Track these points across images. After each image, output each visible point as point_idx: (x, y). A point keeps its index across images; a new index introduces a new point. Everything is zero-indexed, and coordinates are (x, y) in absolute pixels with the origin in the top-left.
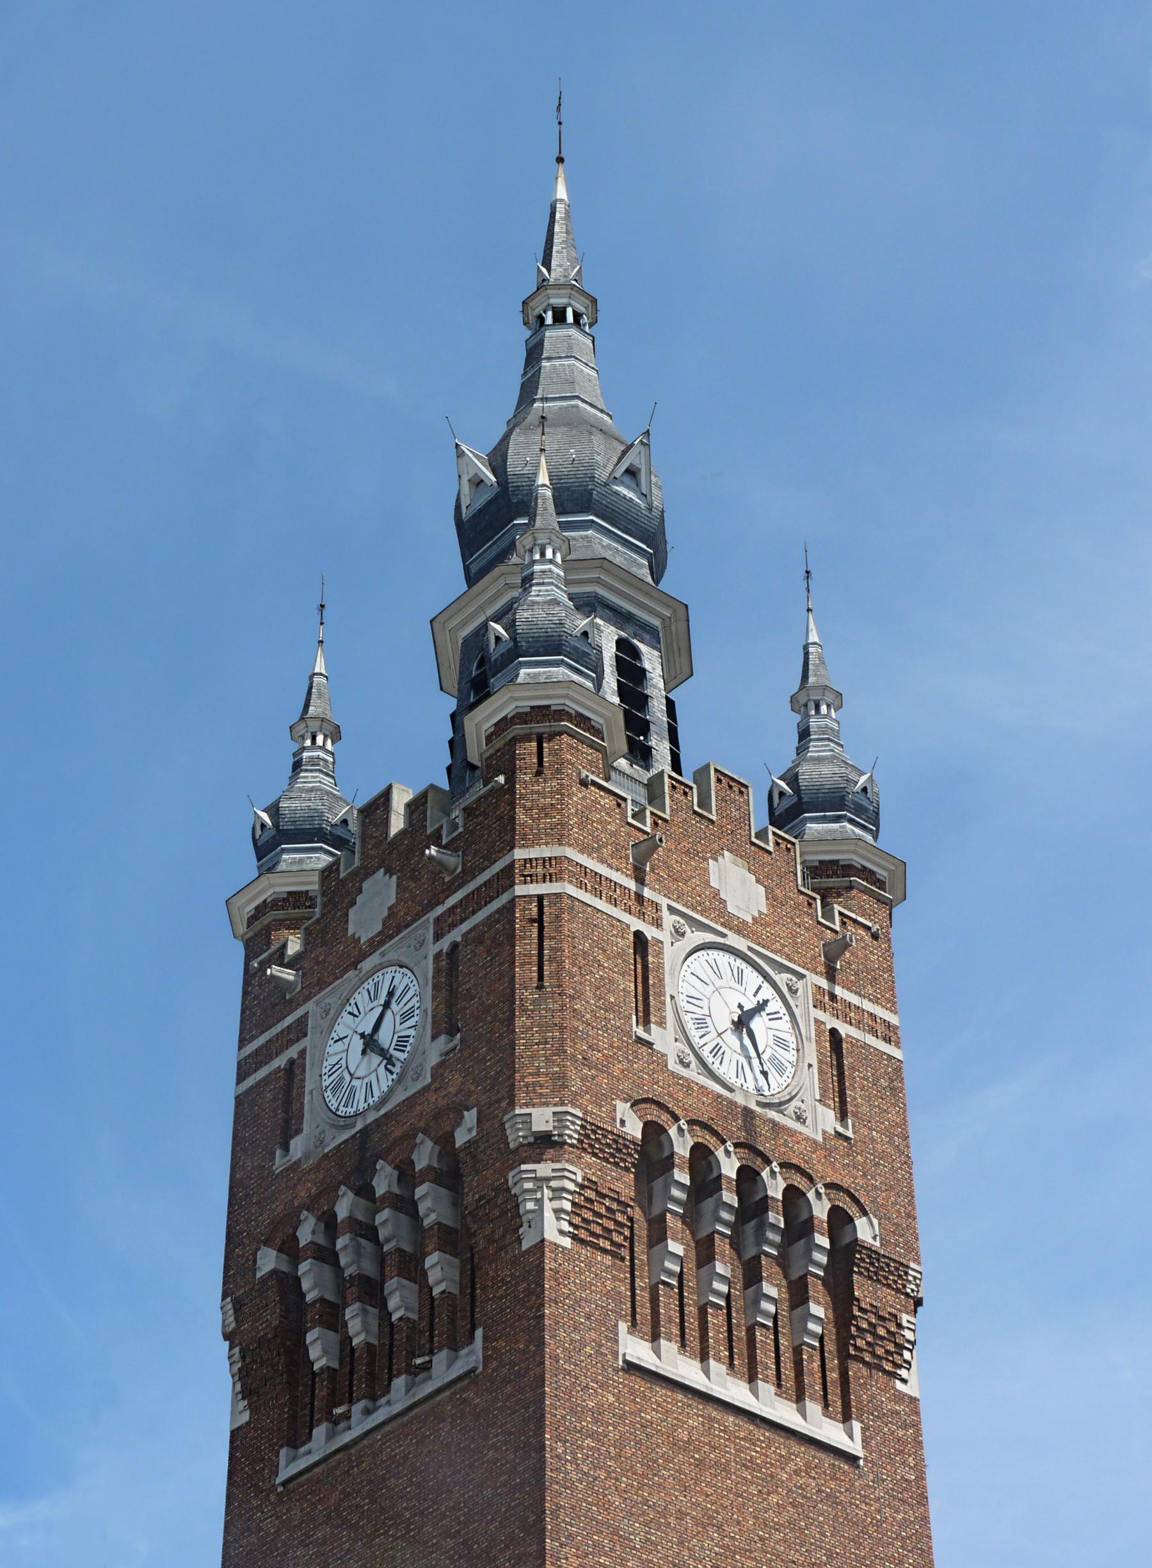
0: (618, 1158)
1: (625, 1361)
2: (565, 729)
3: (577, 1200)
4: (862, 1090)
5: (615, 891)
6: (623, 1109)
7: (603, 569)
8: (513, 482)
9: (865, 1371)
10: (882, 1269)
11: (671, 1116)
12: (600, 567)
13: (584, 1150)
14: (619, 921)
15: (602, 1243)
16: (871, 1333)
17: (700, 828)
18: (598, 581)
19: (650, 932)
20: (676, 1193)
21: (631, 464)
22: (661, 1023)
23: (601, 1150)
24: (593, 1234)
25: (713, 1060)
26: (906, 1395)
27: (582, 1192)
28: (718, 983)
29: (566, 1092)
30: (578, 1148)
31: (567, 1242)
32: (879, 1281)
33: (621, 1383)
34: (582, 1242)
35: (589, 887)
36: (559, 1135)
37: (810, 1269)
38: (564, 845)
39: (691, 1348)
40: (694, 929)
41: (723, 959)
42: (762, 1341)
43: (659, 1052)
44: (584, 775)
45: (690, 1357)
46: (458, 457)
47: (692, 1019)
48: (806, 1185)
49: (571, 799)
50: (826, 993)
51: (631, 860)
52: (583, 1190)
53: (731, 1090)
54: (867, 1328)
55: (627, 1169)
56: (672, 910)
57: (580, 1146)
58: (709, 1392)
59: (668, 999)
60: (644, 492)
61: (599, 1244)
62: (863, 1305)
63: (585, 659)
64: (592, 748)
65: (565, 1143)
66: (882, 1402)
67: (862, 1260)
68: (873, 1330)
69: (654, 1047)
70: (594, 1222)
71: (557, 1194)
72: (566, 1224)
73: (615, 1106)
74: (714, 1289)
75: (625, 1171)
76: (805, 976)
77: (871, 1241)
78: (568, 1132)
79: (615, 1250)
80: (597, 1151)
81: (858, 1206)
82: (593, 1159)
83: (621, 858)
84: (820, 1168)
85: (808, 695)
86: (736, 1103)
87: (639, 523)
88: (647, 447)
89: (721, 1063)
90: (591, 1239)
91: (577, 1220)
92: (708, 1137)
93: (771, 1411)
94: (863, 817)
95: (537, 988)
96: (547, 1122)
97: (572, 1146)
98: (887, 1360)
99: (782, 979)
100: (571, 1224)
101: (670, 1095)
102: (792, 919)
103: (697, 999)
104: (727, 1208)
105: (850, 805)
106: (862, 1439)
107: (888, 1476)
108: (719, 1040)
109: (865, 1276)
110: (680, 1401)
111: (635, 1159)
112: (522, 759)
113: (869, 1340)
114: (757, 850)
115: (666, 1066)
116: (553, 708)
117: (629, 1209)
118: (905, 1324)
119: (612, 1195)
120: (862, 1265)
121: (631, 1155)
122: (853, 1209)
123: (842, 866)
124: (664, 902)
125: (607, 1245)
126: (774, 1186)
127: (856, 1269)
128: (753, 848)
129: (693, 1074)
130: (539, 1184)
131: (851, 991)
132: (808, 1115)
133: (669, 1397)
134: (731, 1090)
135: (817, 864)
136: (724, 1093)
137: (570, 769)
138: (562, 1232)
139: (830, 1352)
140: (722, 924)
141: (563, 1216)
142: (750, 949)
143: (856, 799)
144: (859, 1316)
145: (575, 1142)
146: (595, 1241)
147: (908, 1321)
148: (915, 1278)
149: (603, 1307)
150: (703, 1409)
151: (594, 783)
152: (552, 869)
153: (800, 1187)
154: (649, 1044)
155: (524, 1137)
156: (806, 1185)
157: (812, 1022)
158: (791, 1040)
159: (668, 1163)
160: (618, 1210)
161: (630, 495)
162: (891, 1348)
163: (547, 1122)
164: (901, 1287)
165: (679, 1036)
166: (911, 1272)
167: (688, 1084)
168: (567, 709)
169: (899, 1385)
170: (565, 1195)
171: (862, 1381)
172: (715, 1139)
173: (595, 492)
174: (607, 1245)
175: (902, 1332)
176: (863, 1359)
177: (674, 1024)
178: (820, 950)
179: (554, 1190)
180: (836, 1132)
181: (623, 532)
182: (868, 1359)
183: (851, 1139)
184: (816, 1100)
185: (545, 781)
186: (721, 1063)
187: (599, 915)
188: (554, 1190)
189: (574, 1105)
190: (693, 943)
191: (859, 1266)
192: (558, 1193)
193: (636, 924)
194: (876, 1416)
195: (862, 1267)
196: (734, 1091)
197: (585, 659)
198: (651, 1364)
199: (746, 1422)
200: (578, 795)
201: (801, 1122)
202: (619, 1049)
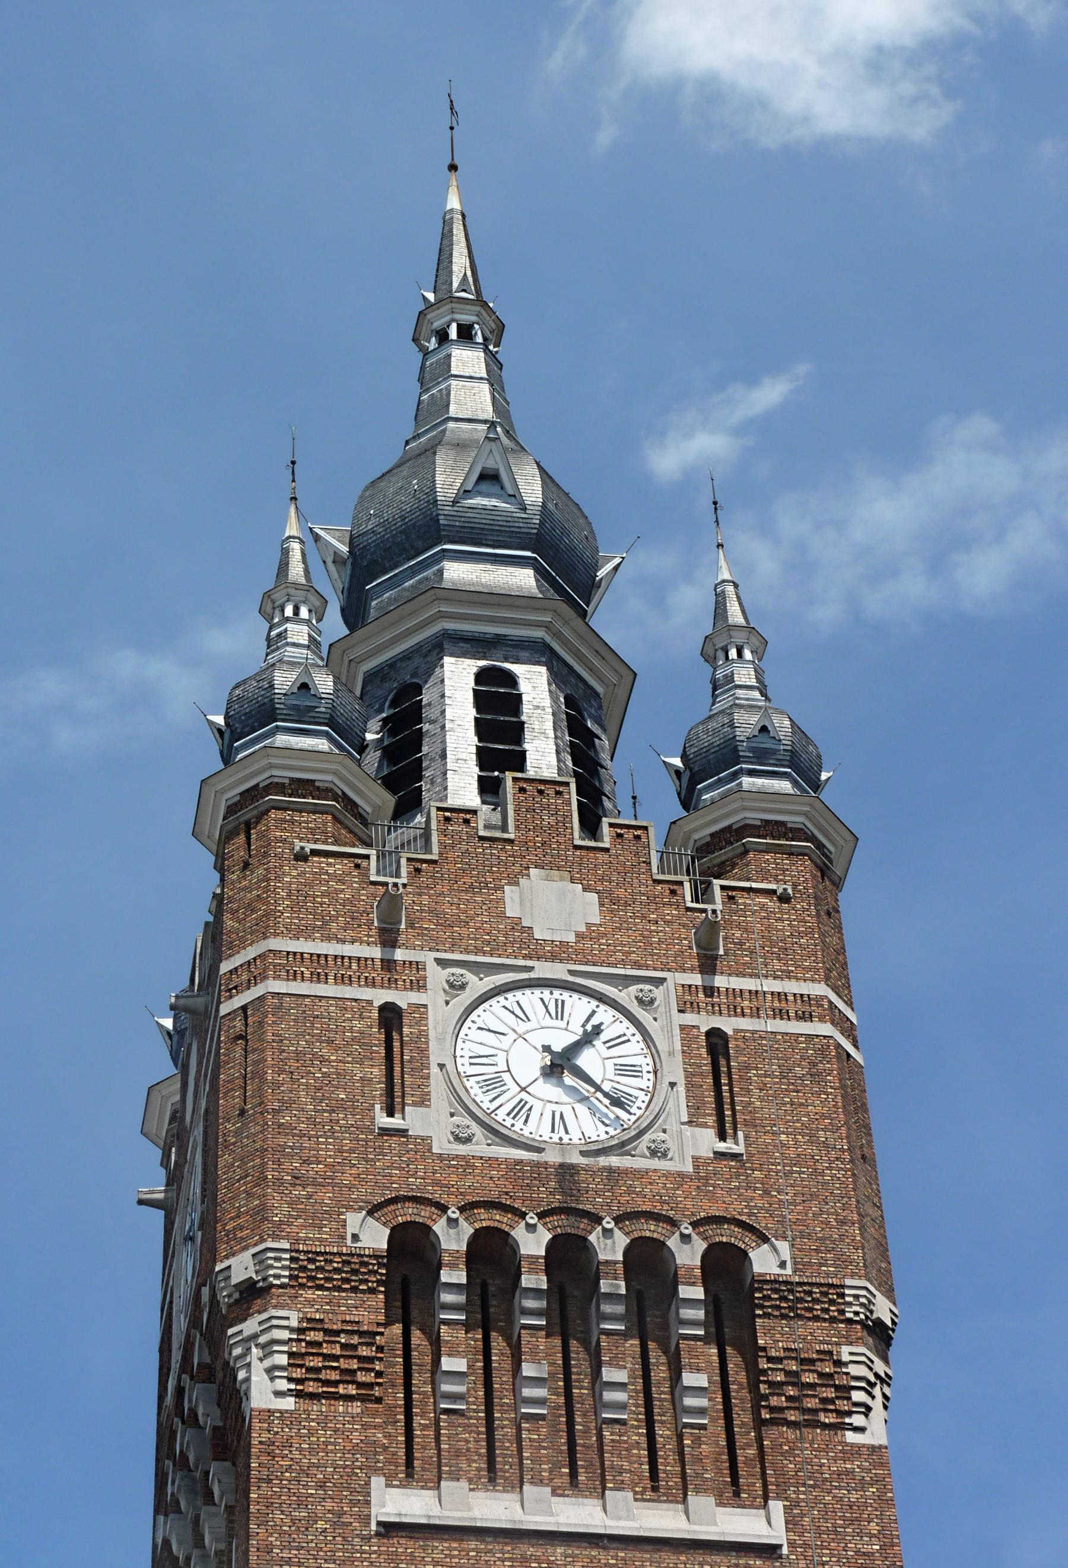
0: (355, 1281)
1: (379, 1523)
2: (271, 804)
3: (294, 1349)
4: (761, 1090)
5: (350, 967)
6: (354, 1220)
7: (441, 599)
8: (359, 545)
9: (791, 1434)
10: (801, 1300)
11: (436, 1208)
12: (437, 599)
13: (302, 1286)
14: (356, 1000)
15: (792, 1416)
16: (793, 1384)
17: (492, 854)
18: (442, 616)
19: (403, 999)
20: (687, 1313)
21: (483, 468)
22: (423, 1101)
23: (327, 1279)
24: (327, 1383)
25: (513, 1122)
26: (864, 1446)
27: (303, 1337)
28: (522, 1027)
29: (267, 1225)
30: (293, 1287)
31: (289, 1403)
32: (799, 1317)
33: (375, 1552)
34: (313, 1396)
35: (307, 974)
36: (264, 1279)
37: (680, 1331)
38: (269, 937)
39: (506, 1479)
40: (482, 976)
41: (530, 998)
42: (613, 1441)
43: (416, 1137)
44: (298, 848)
45: (504, 1491)
46: (316, 541)
47: (478, 1082)
48: (664, 1231)
49: (280, 882)
50: (700, 990)
51: (376, 924)
52: (304, 1334)
53: (540, 1150)
54: (784, 1379)
55: (372, 1291)
56: (441, 963)
57: (295, 1284)
58: (517, 1527)
59: (435, 1070)
60: (512, 493)
61: (338, 1392)
62: (773, 1353)
63: (310, 714)
64: (314, 813)
65: (272, 1286)
66: (822, 1465)
67: (766, 1298)
68: (795, 1380)
69: (410, 1133)
70: (326, 1368)
71: (267, 1350)
72: (285, 1381)
73: (345, 1221)
74: (527, 1398)
75: (370, 1293)
76: (665, 979)
77: (778, 1271)
78: (271, 1272)
79: (364, 1392)
80: (322, 1282)
81: (754, 1234)
82: (317, 1292)
83: (360, 926)
84: (689, 1203)
85: (714, 645)
86: (546, 1163)
87: (512, 529)
88: (498, 442)
89: (526, 1121)
90: (325, 1389)
91: (298, 1373)
92: (498, 1217)
93: (712, 1529)
94: (772, 762)
95: (239, 1115)
96: (246, 1269)
97: (283, 1286)
98: (826, 1410)
99: (626, 996)
100: (290, 1380)
101: (436, 1183)
102: (643, 917)
103: (487, 1056)
104: (532, 1294)
105: (747, 754)
106: (787, 1522)
107: (831, 1556)
108: (524, 1095)
109: (776, 1317)
110: (473, 1550)
111: (382, 1274)
112: (230, 857)
113: (792, 1393)
114: (584, 853)
115: (430, 1150)
116: (261, 785)
117: (378, 1338)
118: (846, 1358)
119: (349, 1328)
120: (766, 1304)
121: (376, 1272)
122: (747, 1240)
123: (737, 830)
124: (428, 958)
125: (352, 1390)
126: (608, 1247)
127: (759, 1312)
128: (578, 853)
129: (482, 1147)
130: (247, 1345)
131: (744, 976)
132: (672, 1145)
133: (455, 1549)
134: (540, 1150)
135: (708, 839)
136: (534, 1156)
137: (280, 847)
138: (278, 1394)
139: (743, 1425)
140: (525, 957)
141: (277, 1374)
142: (571, 972)
143: (754, 745)
144: (769, 1369)
145: (286, 1280)
146: (332, 1390)
147: (851, 1354)
148: (856, 1297)
149: (345, 1467)
150: (513, 1549)
151: (315, 853)
152: (256, 972)
153: (655, 1235)
154: (402, 1133)
155: (229, 1296)
156: (664, 1231)
157: (677, 1031)
158: (645, 1063)
159: (671, 1280)
160: (360, 1344)
161: (494, 502)
162: (830, 1393)
163: (246, 1269)
164: (836, 1314)
165: (456, 1109)
166: (847, 1292)
167: (466, 1163)
168: (276, 780)
169: (851, 1437)
170: (276, 1348)
171: (786, 1448)
172: (510, 1216)
173: (440, 517)
174: (352, 1390)
175: (844, 1370)
176: (786, 1419)
177: (448, 1097)
178: (690, 942)
179: (263, 1347)
180: (715, 1153)
181: (494, 547)
182: (793, 1418)
183: (742, 1155)
184: (683, 1124)
185: (253, 872)
186: (526, 1121)
187: (323, 1003)
188: (263, 1347)
189: (276, 1237)
190: (478, 991)
191: (762, 1307)
192: (267, 1349)
193: (381, 996)
194: (810, 1486)
195: (769, 1307)
196: (544, 1149)
197: (310, 714)
198: (420, 1516)
199: (585, 1548)
200: (292, 874)
201: (659, 1158)
202: (352, 1151)
